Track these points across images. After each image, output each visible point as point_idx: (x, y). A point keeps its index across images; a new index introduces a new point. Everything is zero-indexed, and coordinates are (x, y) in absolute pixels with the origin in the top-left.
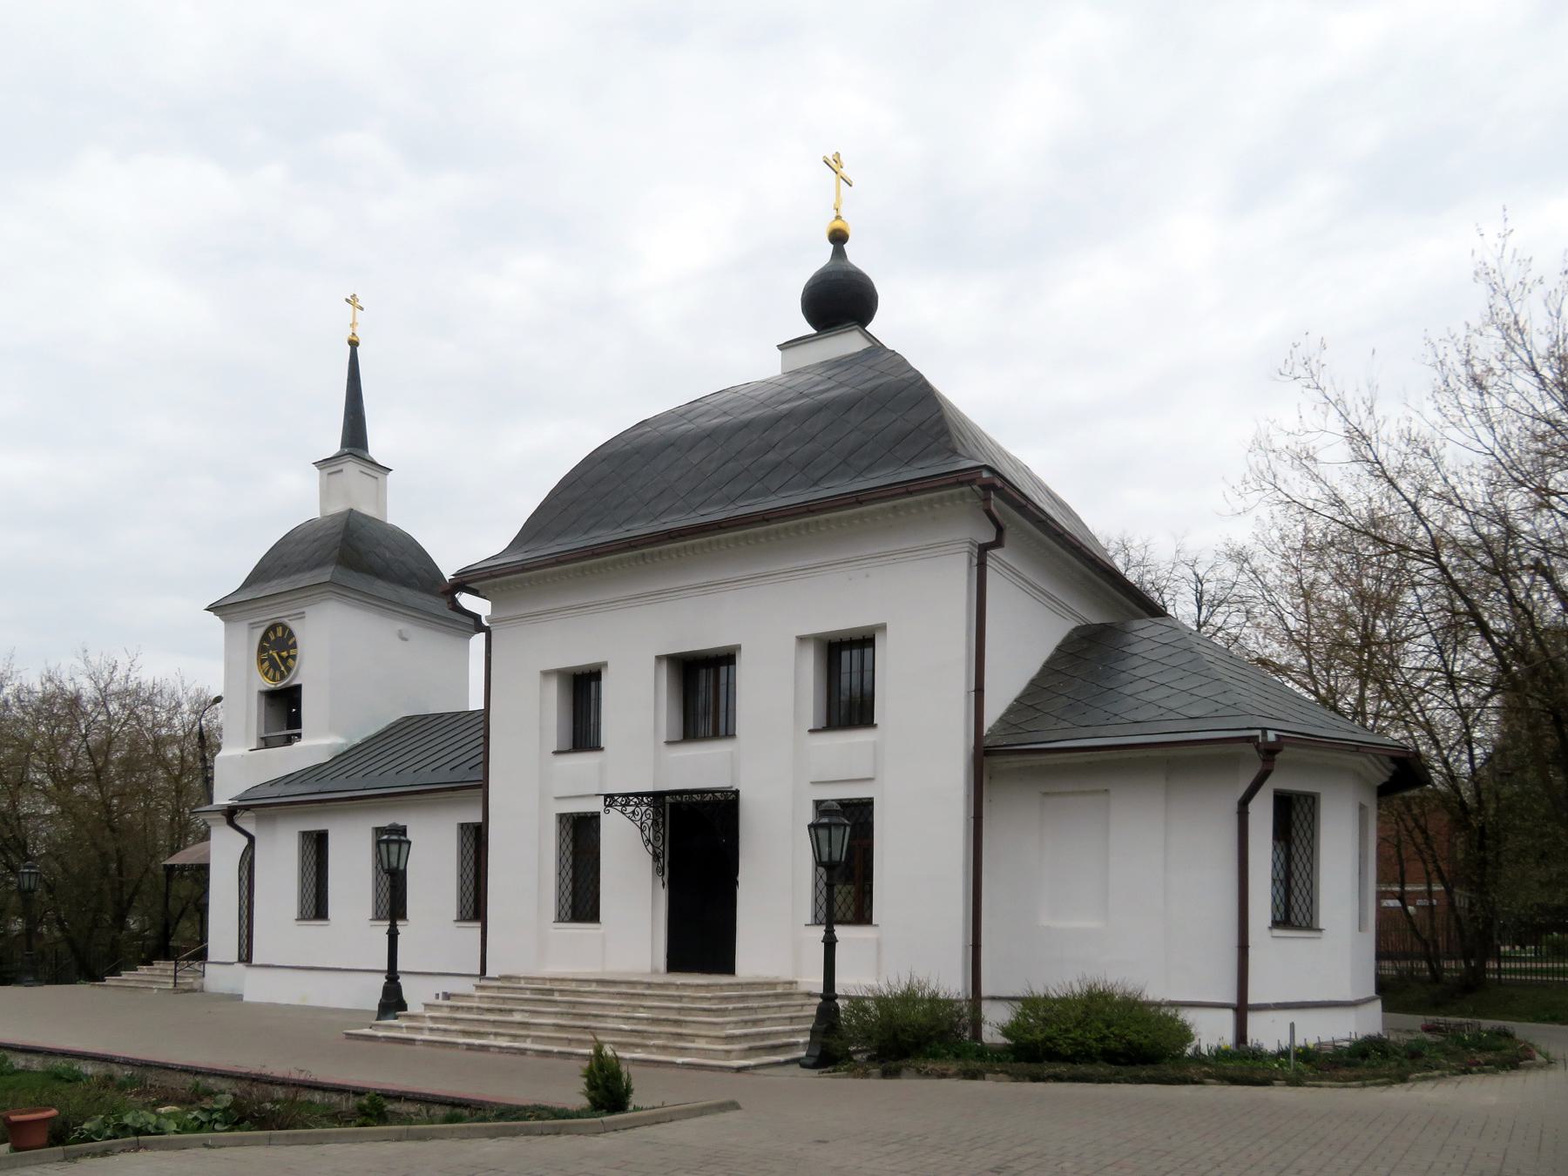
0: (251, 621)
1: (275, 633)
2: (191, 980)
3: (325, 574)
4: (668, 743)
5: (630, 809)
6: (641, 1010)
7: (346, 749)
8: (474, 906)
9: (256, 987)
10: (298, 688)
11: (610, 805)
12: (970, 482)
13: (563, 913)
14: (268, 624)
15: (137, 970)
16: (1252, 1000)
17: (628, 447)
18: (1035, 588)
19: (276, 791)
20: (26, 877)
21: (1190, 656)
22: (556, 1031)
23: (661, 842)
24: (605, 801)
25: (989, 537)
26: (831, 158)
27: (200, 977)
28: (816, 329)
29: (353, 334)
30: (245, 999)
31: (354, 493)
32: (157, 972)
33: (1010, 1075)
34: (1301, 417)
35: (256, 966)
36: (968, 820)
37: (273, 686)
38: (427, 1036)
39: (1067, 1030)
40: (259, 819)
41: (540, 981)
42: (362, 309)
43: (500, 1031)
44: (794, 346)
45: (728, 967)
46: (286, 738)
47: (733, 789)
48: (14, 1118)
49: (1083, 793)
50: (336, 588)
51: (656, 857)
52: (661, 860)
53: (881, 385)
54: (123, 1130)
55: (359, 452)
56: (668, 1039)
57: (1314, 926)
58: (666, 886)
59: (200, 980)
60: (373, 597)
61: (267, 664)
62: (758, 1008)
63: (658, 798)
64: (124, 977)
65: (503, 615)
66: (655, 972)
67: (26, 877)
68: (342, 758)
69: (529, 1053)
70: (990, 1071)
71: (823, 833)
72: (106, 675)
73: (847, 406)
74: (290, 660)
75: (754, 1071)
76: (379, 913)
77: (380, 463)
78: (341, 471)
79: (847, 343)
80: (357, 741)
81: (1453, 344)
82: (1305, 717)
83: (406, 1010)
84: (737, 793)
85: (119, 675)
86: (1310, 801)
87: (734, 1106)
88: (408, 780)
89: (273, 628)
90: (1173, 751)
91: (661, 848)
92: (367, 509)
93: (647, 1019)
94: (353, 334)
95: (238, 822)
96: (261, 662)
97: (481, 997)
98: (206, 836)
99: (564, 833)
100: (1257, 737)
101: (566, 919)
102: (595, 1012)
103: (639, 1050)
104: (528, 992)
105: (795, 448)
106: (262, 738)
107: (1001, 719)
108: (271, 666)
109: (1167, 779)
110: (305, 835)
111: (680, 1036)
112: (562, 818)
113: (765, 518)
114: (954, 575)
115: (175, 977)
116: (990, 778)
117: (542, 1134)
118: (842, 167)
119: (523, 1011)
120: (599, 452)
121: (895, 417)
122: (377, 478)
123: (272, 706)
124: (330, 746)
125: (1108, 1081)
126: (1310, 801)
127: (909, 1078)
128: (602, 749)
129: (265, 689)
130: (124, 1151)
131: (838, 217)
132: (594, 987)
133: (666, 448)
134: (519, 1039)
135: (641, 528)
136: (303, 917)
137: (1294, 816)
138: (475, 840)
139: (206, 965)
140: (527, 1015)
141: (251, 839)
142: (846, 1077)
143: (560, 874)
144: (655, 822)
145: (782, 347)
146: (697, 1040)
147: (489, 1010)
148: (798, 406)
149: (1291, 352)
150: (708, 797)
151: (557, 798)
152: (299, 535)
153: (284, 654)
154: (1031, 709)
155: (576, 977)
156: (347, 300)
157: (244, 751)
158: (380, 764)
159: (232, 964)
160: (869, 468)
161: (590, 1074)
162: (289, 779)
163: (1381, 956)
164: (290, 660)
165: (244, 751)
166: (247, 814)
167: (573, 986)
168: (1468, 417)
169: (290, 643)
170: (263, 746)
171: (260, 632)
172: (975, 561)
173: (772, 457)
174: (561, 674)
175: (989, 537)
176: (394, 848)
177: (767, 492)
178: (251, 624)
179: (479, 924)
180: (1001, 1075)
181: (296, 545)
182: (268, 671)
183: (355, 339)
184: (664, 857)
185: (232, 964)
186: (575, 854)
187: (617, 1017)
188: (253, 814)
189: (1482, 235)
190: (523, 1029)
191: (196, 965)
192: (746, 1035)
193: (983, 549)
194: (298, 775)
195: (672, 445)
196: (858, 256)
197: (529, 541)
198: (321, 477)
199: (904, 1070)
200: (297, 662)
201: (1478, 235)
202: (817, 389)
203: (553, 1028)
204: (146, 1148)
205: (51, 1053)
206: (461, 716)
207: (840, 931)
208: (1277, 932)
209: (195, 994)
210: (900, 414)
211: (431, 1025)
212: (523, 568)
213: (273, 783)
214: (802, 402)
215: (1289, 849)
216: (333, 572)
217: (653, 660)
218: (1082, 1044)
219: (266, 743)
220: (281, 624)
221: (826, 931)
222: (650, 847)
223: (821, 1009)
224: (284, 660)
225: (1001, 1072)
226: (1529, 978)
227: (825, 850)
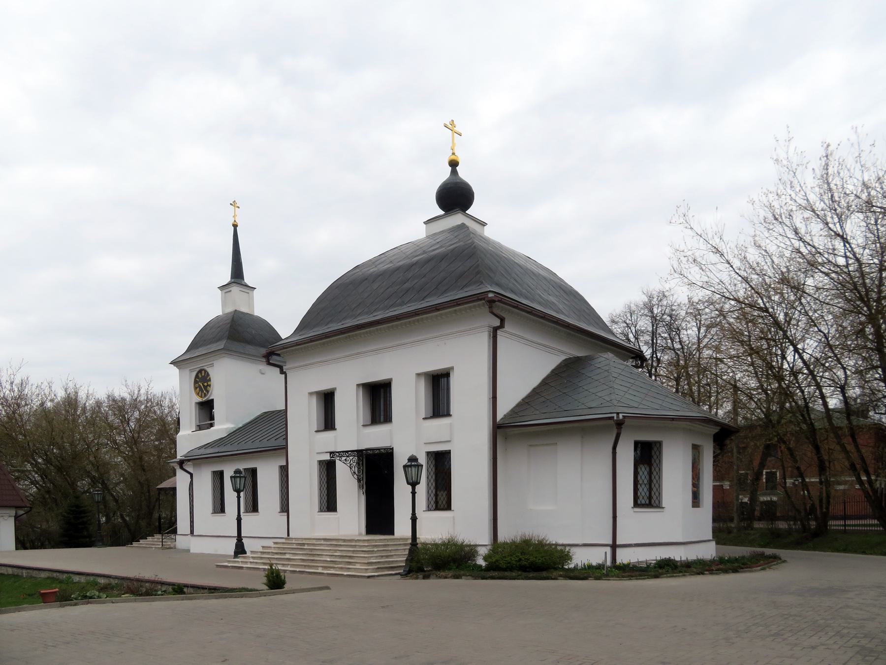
2: (170, 543)
3: (221, 345)
4: (364, 426)
5: (344, 458)
6: (338, 552)
7: (235, 430)
8: (285, 508)
9: (197, 546)
12: (484, 299)
14: (198, 370)
15: (147, 539)
16: (618, 543)
17: (348, 281)
18: (535, 343)
19: (202, 451)
20: (96, 496)
22: (301, 562)
23: (361, 473)
25: (497, 323)
27: (173, 542)
29: (235, 221)
30: (191, 552)
31: (239, 302)
32: (156, 540)
33: (473, 577)
34: (685, 243)
35: (195, 536)
36: (490, 460)
38: (249, 566)
39: (505, 557)
40: (194, 466)
41: (301, 540)
42: (239, 207)
43: (279, 562)
44: (431, 222)
45: (392, 532)
47: (391, 447)
48: (42, 592)
49: (547, 445)
50: (227, 351)
51: (359, 480)
52: (362, 482)
53: (456, 247)
54: (85, 597)
55: (239, 281)
56: (345, 564)
59: (174, 543)
60: (244, 354)
61: (198, 389)
62: (392, 550)
63: (359, 453)
64: (141, 542)
66: (360, 534)
67: (96, 496)
69: (288, 572)
70: (464, 575)
72: (136, 392)
74: (208, 387)
75: (377, 578)
76: (322, 508)
78: (231, 291)
79: (457, 219)
80: (241, 425)
81: (751, 204)
83: (246, 554)
85: (143, 391)
86: (658, 445)
87: (328, 588)
88: (257, 445)
89: (200, 371)
90: (585, 424)
91: (362, 476)
92: (244, 309)
93: (339, 556)
94: (235, 221)
95: (186, 467)
96: (196, 388)
97: (274, 548)
98: (175, 475)
99: (430, 463)
100: (613, 417)
101: (432, 509)
102: (318, 553)
103: (332, 570)
104: (295, 545)
105: (416, 281)
106: (198, 426)
107: (512, 410)
108: (200, 390)
109: (582, 437)
110: (214, 473)
111: (350, 563)
113: (398, 318)
114: (482, 342)
116: (506, 438)
117: (236, 597)
118: (455, 127)
119: (289, 553)
122: (248, 293)
123: (202, 409)
124: (228, 428)
125: (515, 579)
127: (433, 579)
128: (336, 429)
129: (197, 401)
130: (82, 604)
131: (453, 154)
132: (322, 542)
133: (364, 281)
134: (285, 566)
135: (349, 323)
136: (215, 512)
137: (653, 453)
139: (177, 536)
140: (291, 555)
142: (410, 579)
144: (358, 463)
145: (426, 223)
146: (356, 564)
147: (277, 553)
148: (420, 259)
149: (677, 210)
150: (377, 452)
151: (317, 453)
152: (212, 324)
153: (206, 384)
154: (527, 404)
155: (316, 538)
156: (231, 204)
157: (190, 432)
158: (246, 438)
159: (187, 535)
160: (445, 291)
161: (267, 576)
162: (206, 446)
163: (714, 520)
164: (208, 387)
165: (190, 432)
166: (189, 463)
167: (314, 542)
168: (726, 252)
169: (208, 378)
170: (198, 429)
171: (194, 374)
173: (407, 285)
174: (318, 393)
175: (497, 323)
177: (403, 304)
178: (190, 370)
180: (469, 577)
183: (236, 223)
184: (363, 480)
185: (187, 535)
186: (436, 474)
187: (327, 555)
188: (191, 463)
189: (778, 140)
190: (288, 561)
191: (173, 536)
192: (379, 562)
193: (495, 330)
195: (367, 279)
196: (463, 173)
197: (303, 328)
198: (222, 294)
199: (431, 576)
200: (211, 387)
201: (775, 141)
202: (430, 249)
203: (300, 561)
204: (91, 603)
205: (88, 575)
208: (282, 514)
209: (171, 550)
211: (252, 560)
212: (297, 343)
213: (199, 448)
214: (422, 256)
215: (650, 469)
216: (225, 343)
217: (355, 387)
218: (509, 563)
219: (200, 428)
220: (204, 370)
223: (410, 550)
224: (205, 387)
225: (469, 576)
226: (866, 528)
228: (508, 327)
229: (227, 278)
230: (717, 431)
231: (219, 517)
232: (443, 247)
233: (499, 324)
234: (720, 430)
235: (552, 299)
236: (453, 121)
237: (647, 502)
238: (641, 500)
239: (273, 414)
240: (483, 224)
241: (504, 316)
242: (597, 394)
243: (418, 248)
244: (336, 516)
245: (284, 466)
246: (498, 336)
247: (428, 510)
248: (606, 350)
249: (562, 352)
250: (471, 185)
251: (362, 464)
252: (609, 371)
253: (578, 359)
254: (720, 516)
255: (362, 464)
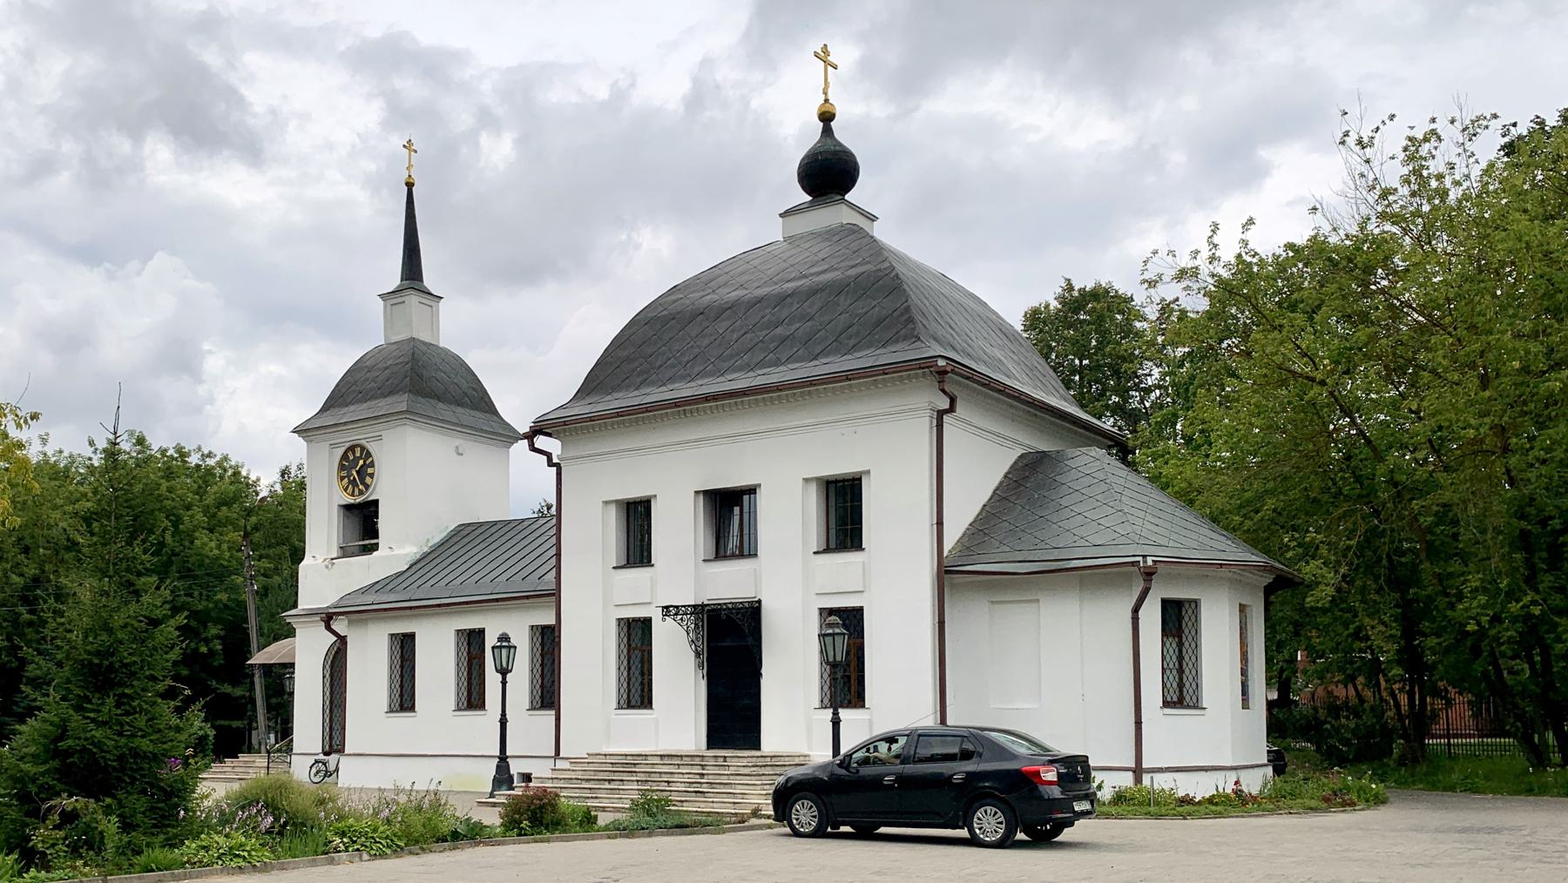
0: (332, 442)
1: (354, 453)
7: (418, 556)
10: (376, 502)
11: (666, 615)
13: (622, 702)
14: (348, 445)
15: (238, 758)
16: (1147, 763)
17: (665, 313)
19: (369, 598)
21: (1104, 487)
24: (663, 611)
26: (819, 51)
28: (810, 194)
29: (410, 176)
37: (352, 501)
42: (416, 152)
46: (362, 548)
47: (757, 599)
50: (410, 414)
51: (698, 654)
55: (416, 284)
57: (1200, 706)
58: (705, 678)
63: (698, 610)
65: (571, 454)
68: (419, 566)
71: (829, 640)
73: (839, 289)
77: (435, 294)
78: (404, 302)
79: (831, 216)
82: (1183, 540)
84: (759, 602)
86: (1193, 606)
89: (352, 449)
92: (425, 336)
94: (410, 176)
100: (1139, 562)
105: (798, 325)
108: (350, 482)
112: (619, 620)
115: (268, 768)
120: (641, 316)
121: (874, 303)
123: (348, 517)
124: (406, 555)
126: (1193, 606)
128: (653, 565)
129: (344, 503)
138: (548, 641)
139: (293, 756)
141: (342, 640)
143: (619, 669)
145: (781, 215)
156: (404, 146)
160: (854, 348)
171: (340, 452)
172: (935, 421)
175: (947, 406)
176: (504, 652)
179: (553, 712)
181: (369, 371)
182: (348, 487)
183: (412, 181)
193: (941, 414)
194: (384, 583)
206: (512, 525)
207: (844, 714)
210: (877, 301)
213: (364, 591)
214: (800, 283)
219: (345, 552)
221: (834, 714)
222: (693, 646)
227: (831, 654)
228: (960, 409)
229: (394, 279)
230: (1271, 581)
231: (472, 717)
232: (836, 269)
233: (947, 407)
234: (1274, 579)
235: (998, 354)
236: (825, 45)
237: (1175, 699)
238: (633, 703)
239: (506, 529)
240: (872, 218)
241: (956, 393)
242: (1100, 521)
243: (786, 265)
244: (650, 716)
245: (548, 627)
246: (944, 424)
247: (822, 708)
248: (1089, 443)
249: (1015, 442)
250: (854, 151)
251: (703, 626)
252: (1107, 481)
253: (1043, 455)
254: (1281, 723)
255: (703, 626)
